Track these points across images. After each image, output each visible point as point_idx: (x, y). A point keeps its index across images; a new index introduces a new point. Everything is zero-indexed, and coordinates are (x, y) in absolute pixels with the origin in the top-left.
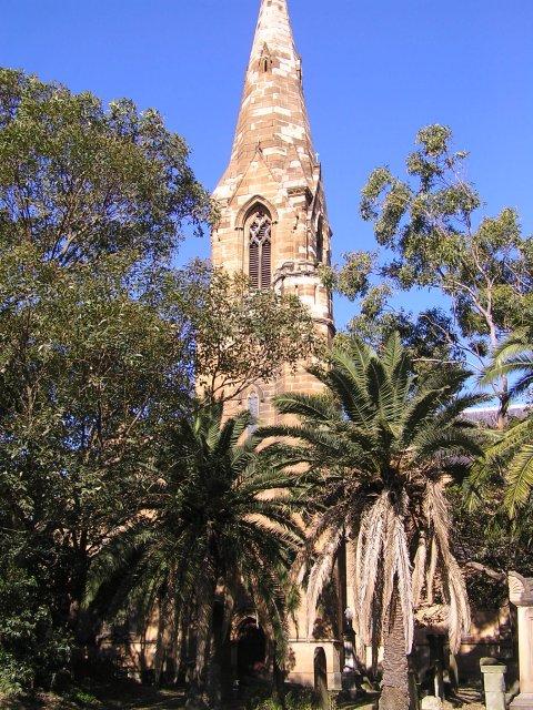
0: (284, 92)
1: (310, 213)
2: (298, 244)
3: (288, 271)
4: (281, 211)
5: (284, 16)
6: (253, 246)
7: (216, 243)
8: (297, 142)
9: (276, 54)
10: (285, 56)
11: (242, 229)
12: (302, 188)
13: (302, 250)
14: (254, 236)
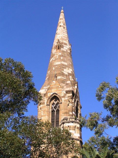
0: (65, 57)
1: (74, 100)
3: (65, 121)
4: (63, 99)
6: (53, 111)
7: (40, 110)
8: (69, 74)
9: (62, 43)
10: (66, 44)
11: (49, 105)
13: (71, 113)
14: (53, 108)
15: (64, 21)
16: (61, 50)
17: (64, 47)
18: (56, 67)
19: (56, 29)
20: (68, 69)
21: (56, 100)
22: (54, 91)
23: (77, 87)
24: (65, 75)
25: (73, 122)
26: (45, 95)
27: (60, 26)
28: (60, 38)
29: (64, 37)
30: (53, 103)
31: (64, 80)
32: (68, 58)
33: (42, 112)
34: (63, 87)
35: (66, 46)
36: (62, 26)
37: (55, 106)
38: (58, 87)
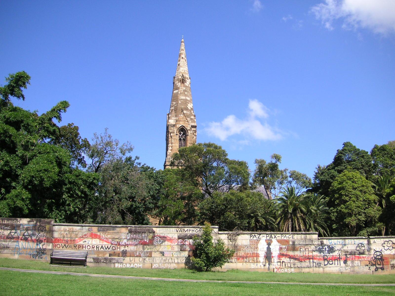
5: (186, 63)
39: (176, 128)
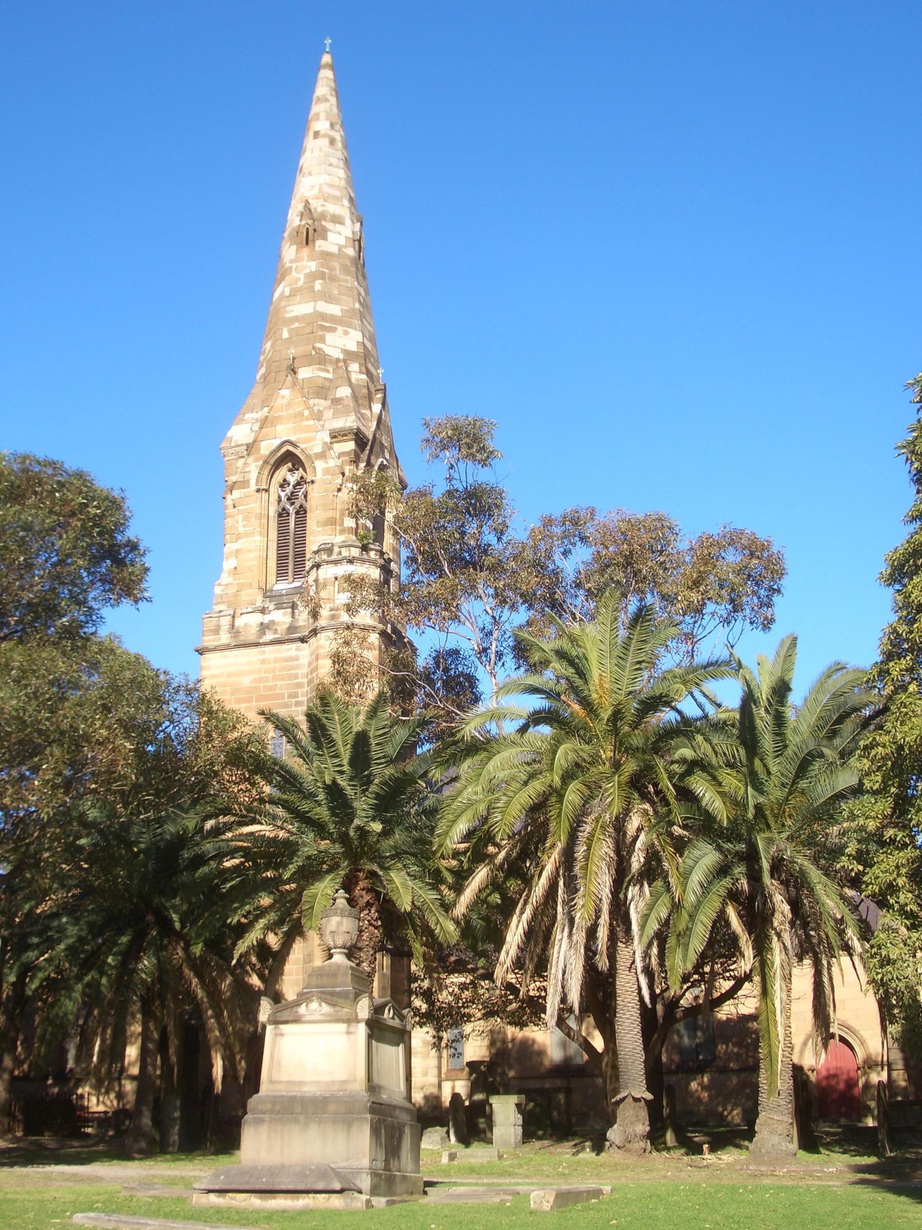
0: (333, 279)
1: (362, 465)
2: (342, 515)
3: (325, 557)
4: (319, 465)
5: (337, 155)
6: (283, 514)
7: (230, 511)
8: (349, 356)
9: (323, 216)
10: (337, 220)
11: (267, 490)
12: (350, 430)
13: (350, 523)
14: (284, 499)
15: (335, 110)
16: (317, 248)
17: (329, 234)
18: (297, 325)
19: (298, 150)
20: (346, 333)
21: (294, 466)
22: (282, 432)
23: (380, 406)
24: (331, 362)
25: (351, 561)
26: (250, 448)
27: (317, 134)
28: (316, 191)
29: (331, 186)
30: (285, 480)
31: (327, 384)
32: (346, 281)
33: (240, 517)
34: (320, 412)
35: (339, 227)
36: (325, 136)
37: (292, 493)
38: (299, 416)
39: (256, 460)
